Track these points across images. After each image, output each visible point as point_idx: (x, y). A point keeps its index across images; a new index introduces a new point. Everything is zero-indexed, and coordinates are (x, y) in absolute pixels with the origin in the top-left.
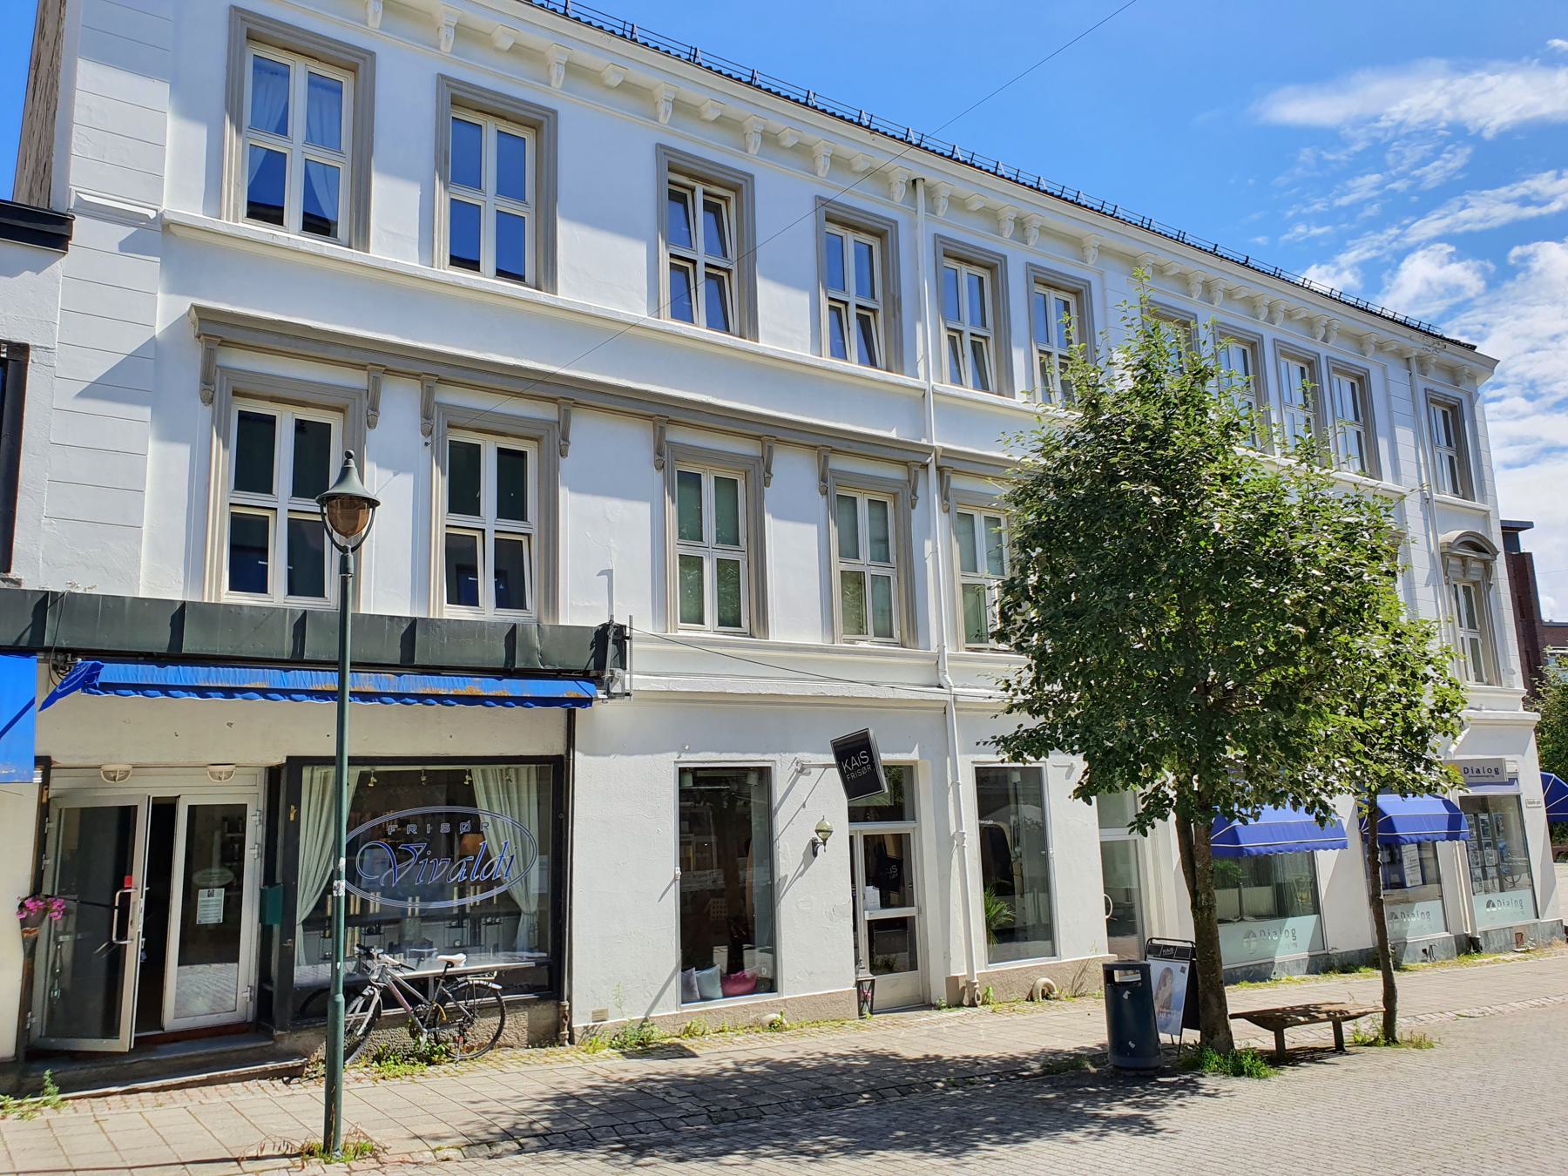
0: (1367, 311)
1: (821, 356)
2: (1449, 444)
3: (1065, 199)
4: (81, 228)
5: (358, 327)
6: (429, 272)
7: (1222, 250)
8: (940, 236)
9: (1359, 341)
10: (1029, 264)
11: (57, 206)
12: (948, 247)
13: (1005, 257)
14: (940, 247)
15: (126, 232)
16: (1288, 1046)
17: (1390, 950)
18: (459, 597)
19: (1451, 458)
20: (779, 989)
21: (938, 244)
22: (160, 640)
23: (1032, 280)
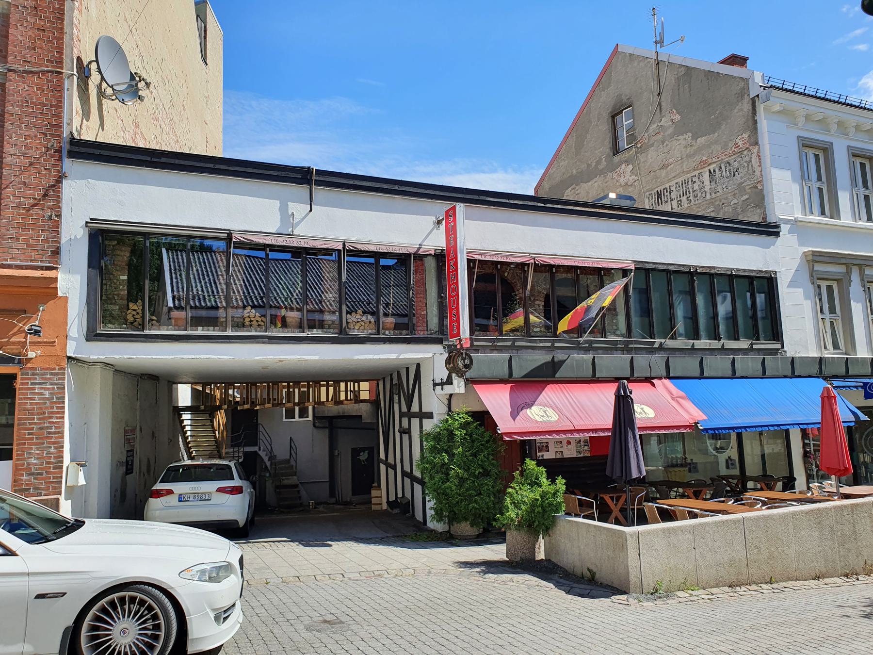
0: (805, 94)
1: (806, 216)
2: (819, 179)
3: (809, 95)
4: (784, 229)
5: (839, 249)
6: (811, 218)
7: (810, 89)
8: (800, 137)
9: (823, 122)
10: (798, 137)
11: (771, 219)
12: (805, 142)
13: (832, 143)
14: (801, 142)
15: (84, 121)
16: (189, 404)
17: (582, 455)
18: (774, 337)
19: (820, 190)
20: (431, 411)
21: (800, 141)
22: (842, 371)
23: (801, 145)
